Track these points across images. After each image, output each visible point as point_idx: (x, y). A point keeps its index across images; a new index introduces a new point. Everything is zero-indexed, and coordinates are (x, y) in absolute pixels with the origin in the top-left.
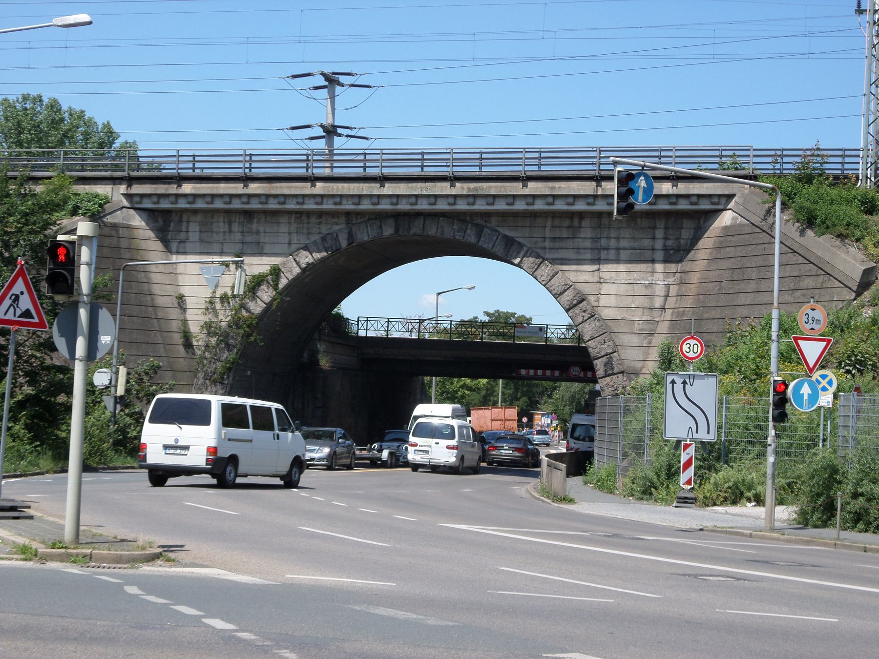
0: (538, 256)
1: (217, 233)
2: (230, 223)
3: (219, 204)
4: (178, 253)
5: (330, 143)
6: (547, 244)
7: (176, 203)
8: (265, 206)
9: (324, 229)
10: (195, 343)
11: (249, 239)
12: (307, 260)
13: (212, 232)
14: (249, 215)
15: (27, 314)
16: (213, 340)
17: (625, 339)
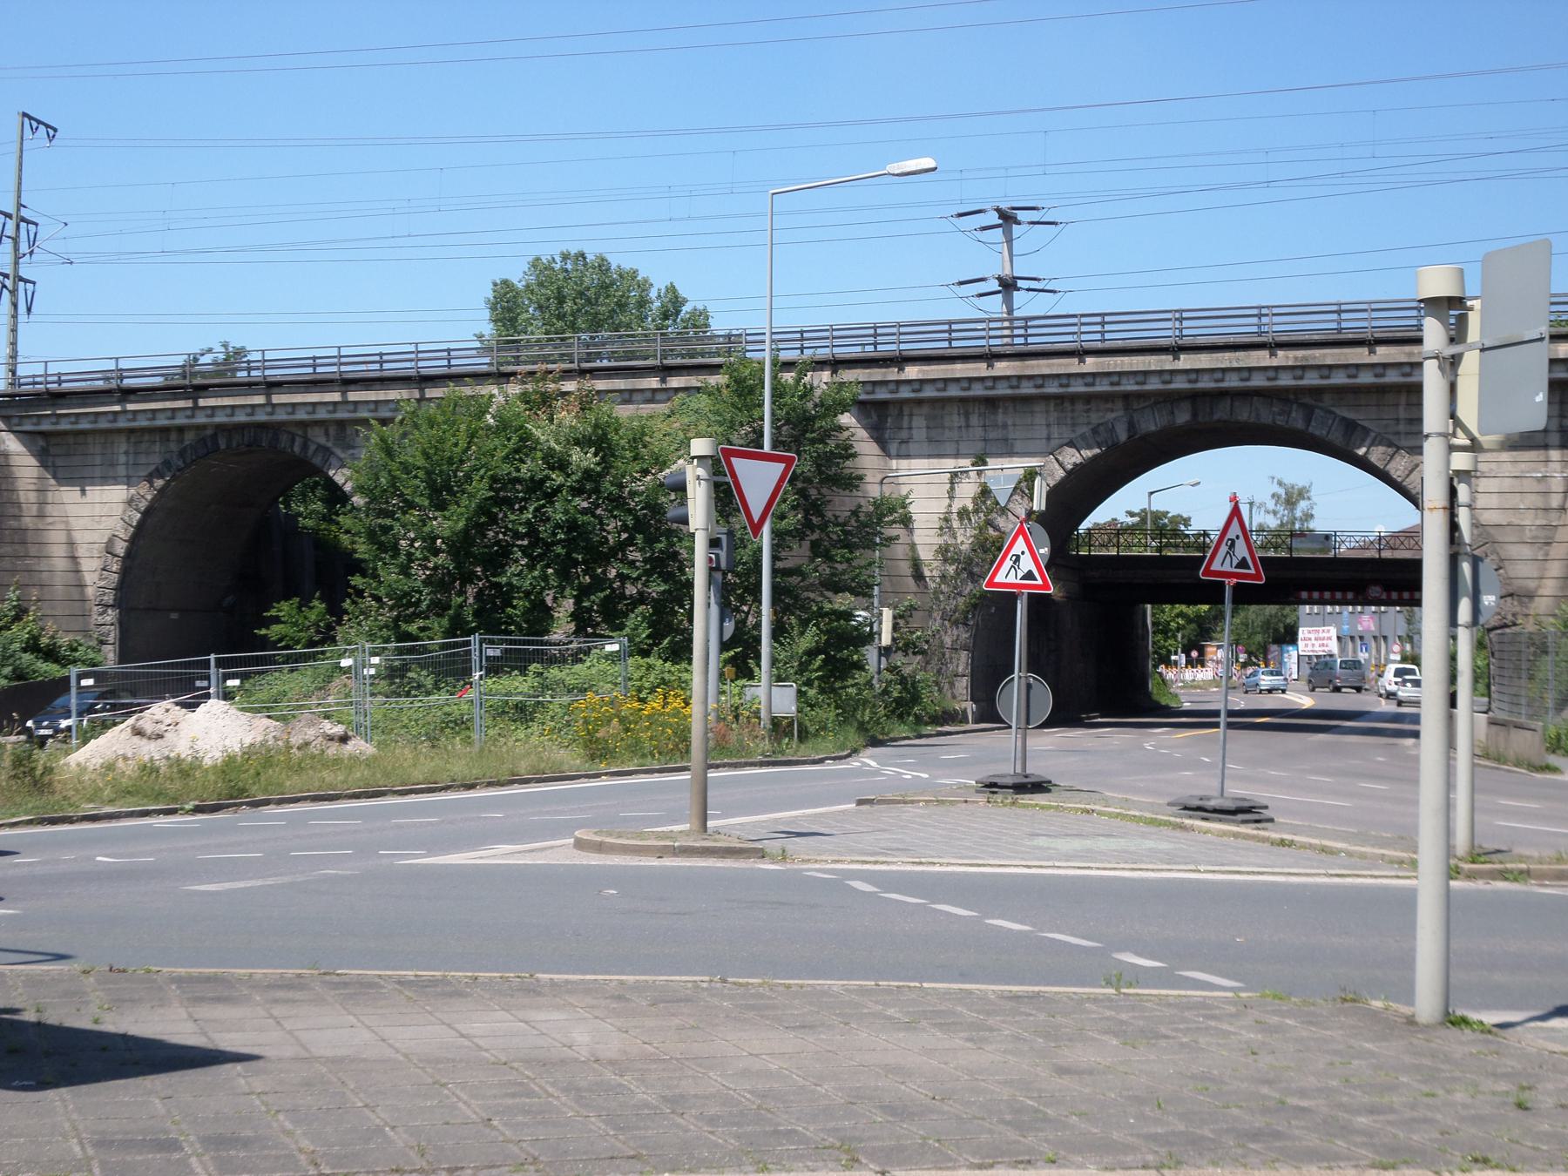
0: (1390, 445)
1: (950, 429)
2: (967, 415)
3: (953, 391)
4: (899, 456)
5: (1008, 302)
6: (1402, 427)
7: (897, 391)
8: (1017, 391)
9: (1095, 418)
10: (927, 573)
11: (992, 435)
12: (1073, 460)
13: (943, 427)
14: (991, 403)
15: (1029, 576)
16: (951, 569)
17: (1514, 551)
